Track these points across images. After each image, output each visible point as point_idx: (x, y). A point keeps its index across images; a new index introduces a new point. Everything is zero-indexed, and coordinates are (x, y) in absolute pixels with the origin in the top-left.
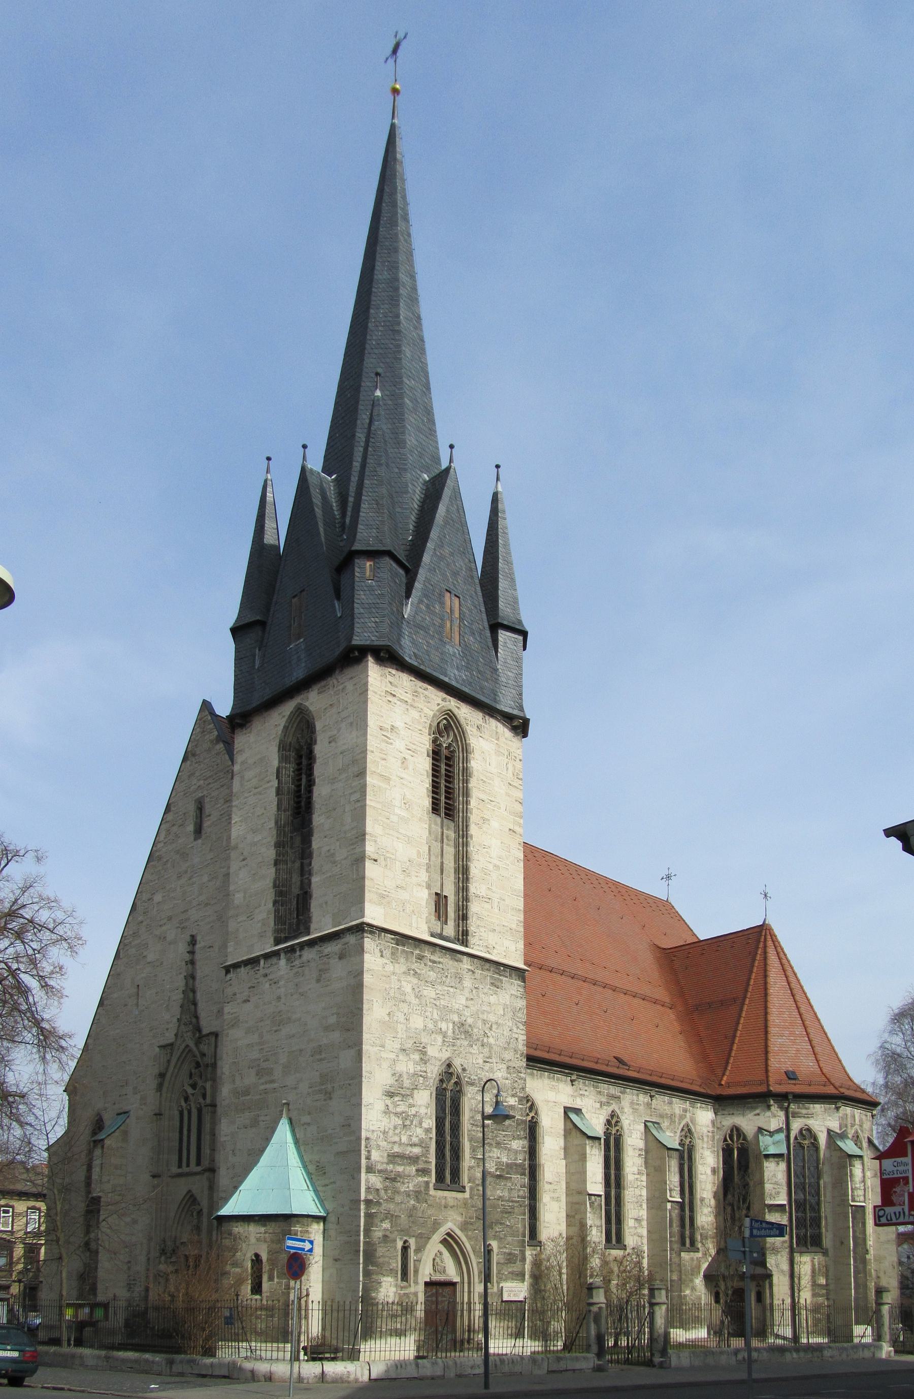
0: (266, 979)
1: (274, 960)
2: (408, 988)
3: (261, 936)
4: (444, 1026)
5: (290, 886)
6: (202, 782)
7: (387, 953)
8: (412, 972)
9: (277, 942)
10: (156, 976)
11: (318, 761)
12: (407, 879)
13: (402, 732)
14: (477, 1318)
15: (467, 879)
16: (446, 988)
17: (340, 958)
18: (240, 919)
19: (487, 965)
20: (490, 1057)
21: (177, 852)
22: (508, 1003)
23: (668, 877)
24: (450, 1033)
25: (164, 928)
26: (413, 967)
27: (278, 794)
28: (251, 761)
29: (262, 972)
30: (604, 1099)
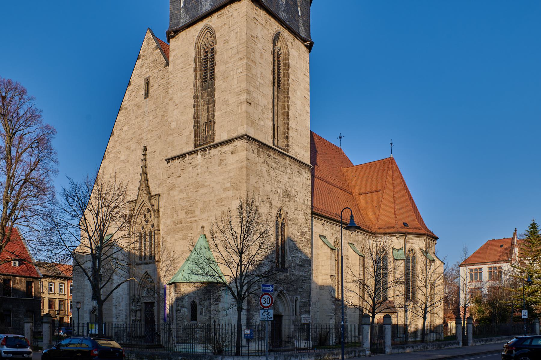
0: (190, 165)
1: (194, 155)
4: (279, 190)
6: (148, 69)
7: (256, 151)
9: (196, 146)
12: (263, 115)
13: (261, 40)
15: (288, 119)
17: (232, 154)
18: (174, 135)
21: (136, 105)
23: (341, 137)
24: (281, 195)
25: (129, 143)
27: (195, 71)
28: (179, 55)
29: (187, 162)
30: (334, 232)
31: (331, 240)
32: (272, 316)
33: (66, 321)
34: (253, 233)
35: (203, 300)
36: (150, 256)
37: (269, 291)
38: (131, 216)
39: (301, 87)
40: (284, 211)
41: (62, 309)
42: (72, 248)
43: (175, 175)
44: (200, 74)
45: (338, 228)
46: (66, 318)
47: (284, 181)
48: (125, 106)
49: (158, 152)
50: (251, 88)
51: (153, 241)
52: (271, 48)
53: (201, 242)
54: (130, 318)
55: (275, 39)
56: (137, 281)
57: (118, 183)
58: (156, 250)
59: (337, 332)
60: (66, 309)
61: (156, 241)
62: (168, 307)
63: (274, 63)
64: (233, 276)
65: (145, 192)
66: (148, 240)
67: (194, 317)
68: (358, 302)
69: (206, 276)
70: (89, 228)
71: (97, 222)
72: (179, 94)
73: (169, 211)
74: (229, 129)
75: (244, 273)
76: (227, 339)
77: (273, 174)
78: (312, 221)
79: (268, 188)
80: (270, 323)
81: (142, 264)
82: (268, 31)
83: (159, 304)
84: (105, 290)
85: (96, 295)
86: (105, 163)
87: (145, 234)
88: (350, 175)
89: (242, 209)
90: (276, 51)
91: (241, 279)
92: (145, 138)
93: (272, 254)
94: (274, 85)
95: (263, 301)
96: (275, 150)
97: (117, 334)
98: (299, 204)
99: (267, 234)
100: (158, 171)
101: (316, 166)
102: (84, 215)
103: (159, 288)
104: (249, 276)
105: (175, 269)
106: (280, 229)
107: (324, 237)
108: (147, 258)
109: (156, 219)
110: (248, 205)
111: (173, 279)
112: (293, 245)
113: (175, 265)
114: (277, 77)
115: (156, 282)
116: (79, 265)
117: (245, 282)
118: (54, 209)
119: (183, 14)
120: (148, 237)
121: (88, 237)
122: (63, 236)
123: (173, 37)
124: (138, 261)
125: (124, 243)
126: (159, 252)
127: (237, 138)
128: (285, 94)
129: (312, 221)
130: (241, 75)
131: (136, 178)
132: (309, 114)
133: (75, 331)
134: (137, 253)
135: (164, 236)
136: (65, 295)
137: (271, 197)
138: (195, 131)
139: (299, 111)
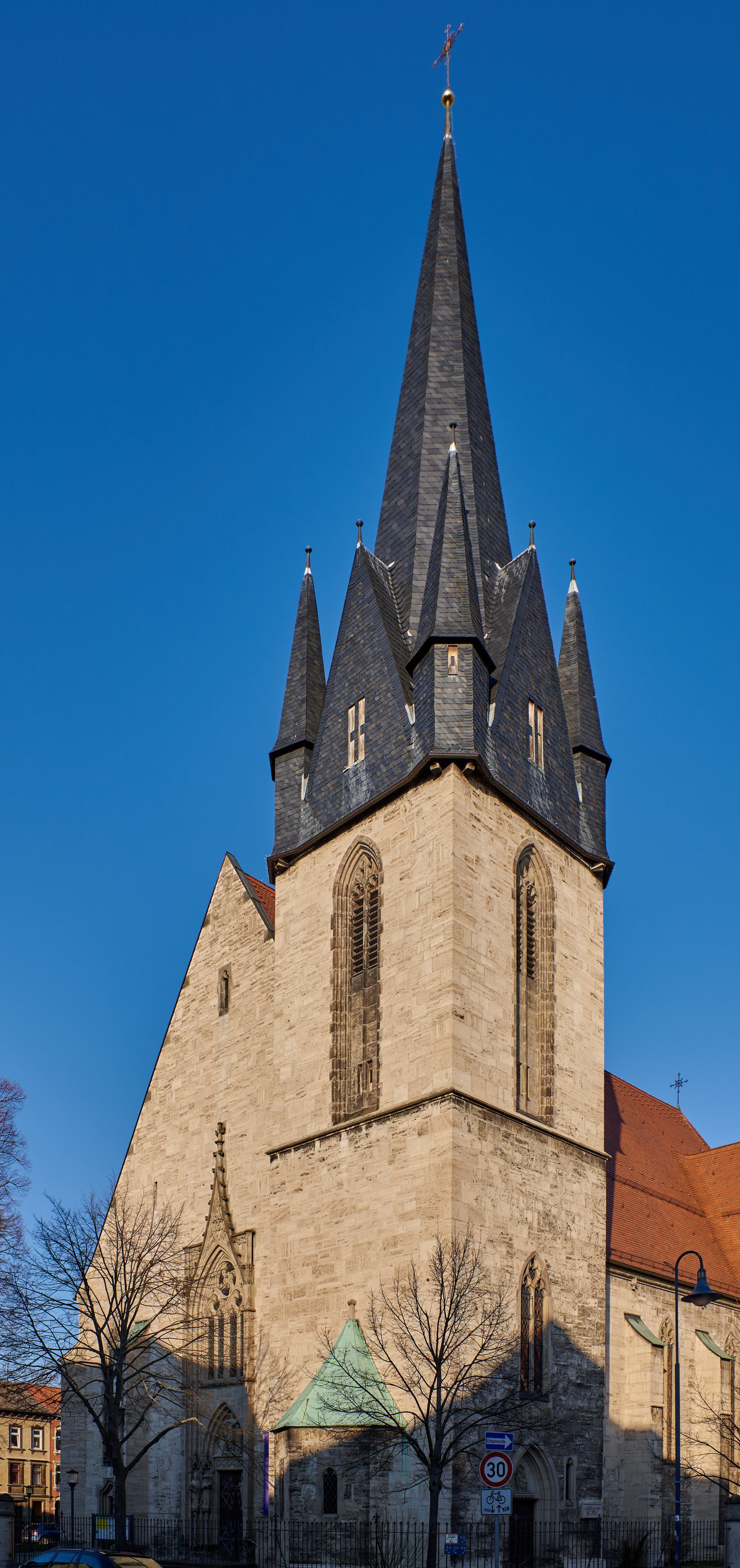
1: (333, 1141)
2: (495, 1171)
3: (315, 1115)
4: (529, 1215)
5: (350, 1056)
6: (227, 948)
7: (475, 1127)
8: (499, 1152)
9: (336, 1120)
10: (177, 1171)
11: (385, 902)
12: (493, 1043)
13: (488, 866)
14: (557, 1537)
15: (552, 1048)
16: (532, 1173)
17: (420, 1134)
18: (287, 1097)
19: (570, 1149)
20: (572, 1253)
21: (199, 1030)
22: (590, 1193)
23: (679, 1083)
24: (535, 1225)
25: (185, 1117)
26: (500, 1146)
27: (333, 947)
28: (297, 912)
29: (317, 1156)
30: (660, 1306)
31: (653, 1325)
32: (508, 1503)
33: (48, 1510)
34: (467, 1314)
35: (351, 1466)
36: (234, 1370)
37: (502, 1447)
38: (190, 1280)
39: (584, 970)
40: (541, 1262)
41: (39, 1483)
42: (58, 1352)
43: (289, 1188)
44: (346, 954)
45: (670, 1297)
46: (47, 1504)
47: (542, 1194)
48: (175, 1034)
49: (250, 1136)
50: (465, 981)
51: (239, 1335)
52: (512, 885)
53: (348, 1338)
54: (187, 1505)
55: (520, 862)
56: (203, 1424)
57: (160, 1207)
58: (245, 1355)
59: (666, 1538)
60: (48, 1484)
61: (246, 1335)
62: (272, 1481)
63: (518, 918)
64: (419, 1413)
65: (222, 1225)
66: (227, 1333)
67: (330, 1505)
68: (717, 1468)
69: (357, 1415)
70: (96, 1308)
71: (115, 1296)
72: (298, 1002)
73: (274, 1268)
74: (413, 1079)
75: (447, 1406)
76: (405, 1554)
77: (516, 1177)
78: (608, 1281)
79: (504, 1210)
80: (507, 1520)
81: (214, 1386)
82: (505, 843)
83: (251, 1477)
84: (132, 1444)
85: (111, 1456)
86: (132, 1162)
87: (221, 1321)
88: (702, 1171)
89: (441, 1263)
90: (524, 891)
91: (437, 1419)
92: (220, 1105)
93: (512, 1361)
94: (519, 971)
95: (487, 1470)
96: (524, 1123)
97: (157, 1542)
98: (578, 1244)
99: (499, 1316)
100: (250, 1179)
101: (618, 1155)
102: (85, 1280)
103: (252, 1441)
104: (457, 1411)
105: (289, 1398)
106: (532, 1303)
107: (637, 1318)
108: (226, 1374)
109: (246, 1287)
110: (456, 1252)
111: (283, 1419)
112: (563, 1339)
113: (289, 1389)
114: (525, 951)
115: (244, 1425)
116: (74, 1390)
117: (449, 1425)
118: (19, 1267)
119: (305, 815)
120: (227, 1327)
121: (95, 1330)
122: (39, 1327)
123: (283, 871)
124: (205, 1379)
125: (174, 1341)
126: (252, 1359)
127: (432, 1098)
128: (544, 990)
129: (608, 1281)
130: (441, 950)
131: (200, 1194)
132: (602, 1035)
133: (65, 1533)
134: (204, 1362)
135: (265, 1323)
136: (44, 1452)
137: (512, 1230)
138: (335, 1085)
139: (577, 1029)
